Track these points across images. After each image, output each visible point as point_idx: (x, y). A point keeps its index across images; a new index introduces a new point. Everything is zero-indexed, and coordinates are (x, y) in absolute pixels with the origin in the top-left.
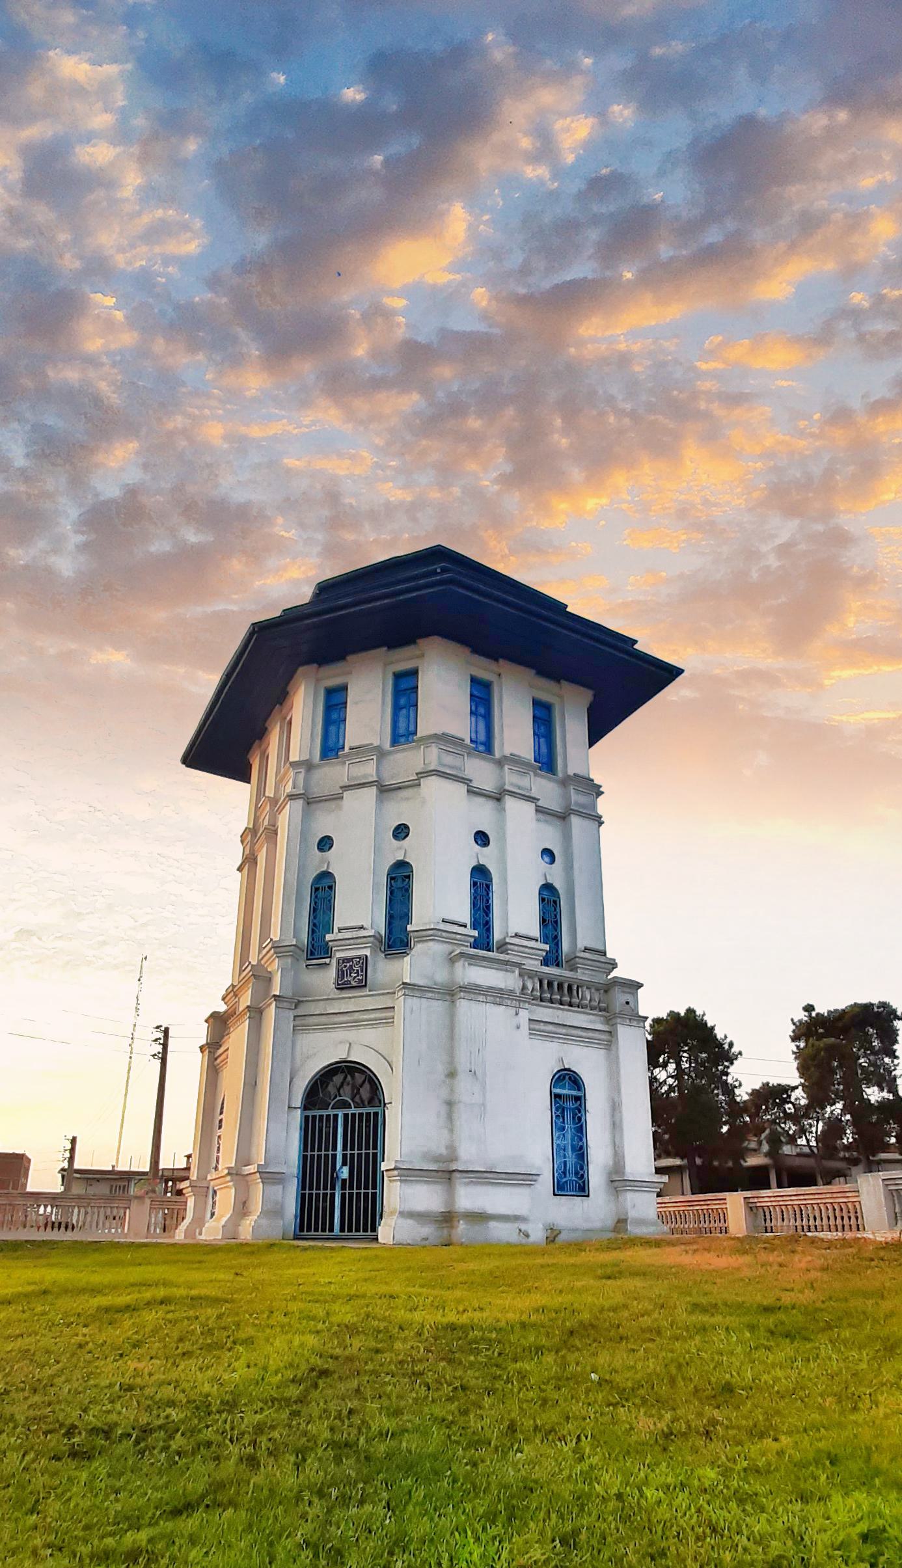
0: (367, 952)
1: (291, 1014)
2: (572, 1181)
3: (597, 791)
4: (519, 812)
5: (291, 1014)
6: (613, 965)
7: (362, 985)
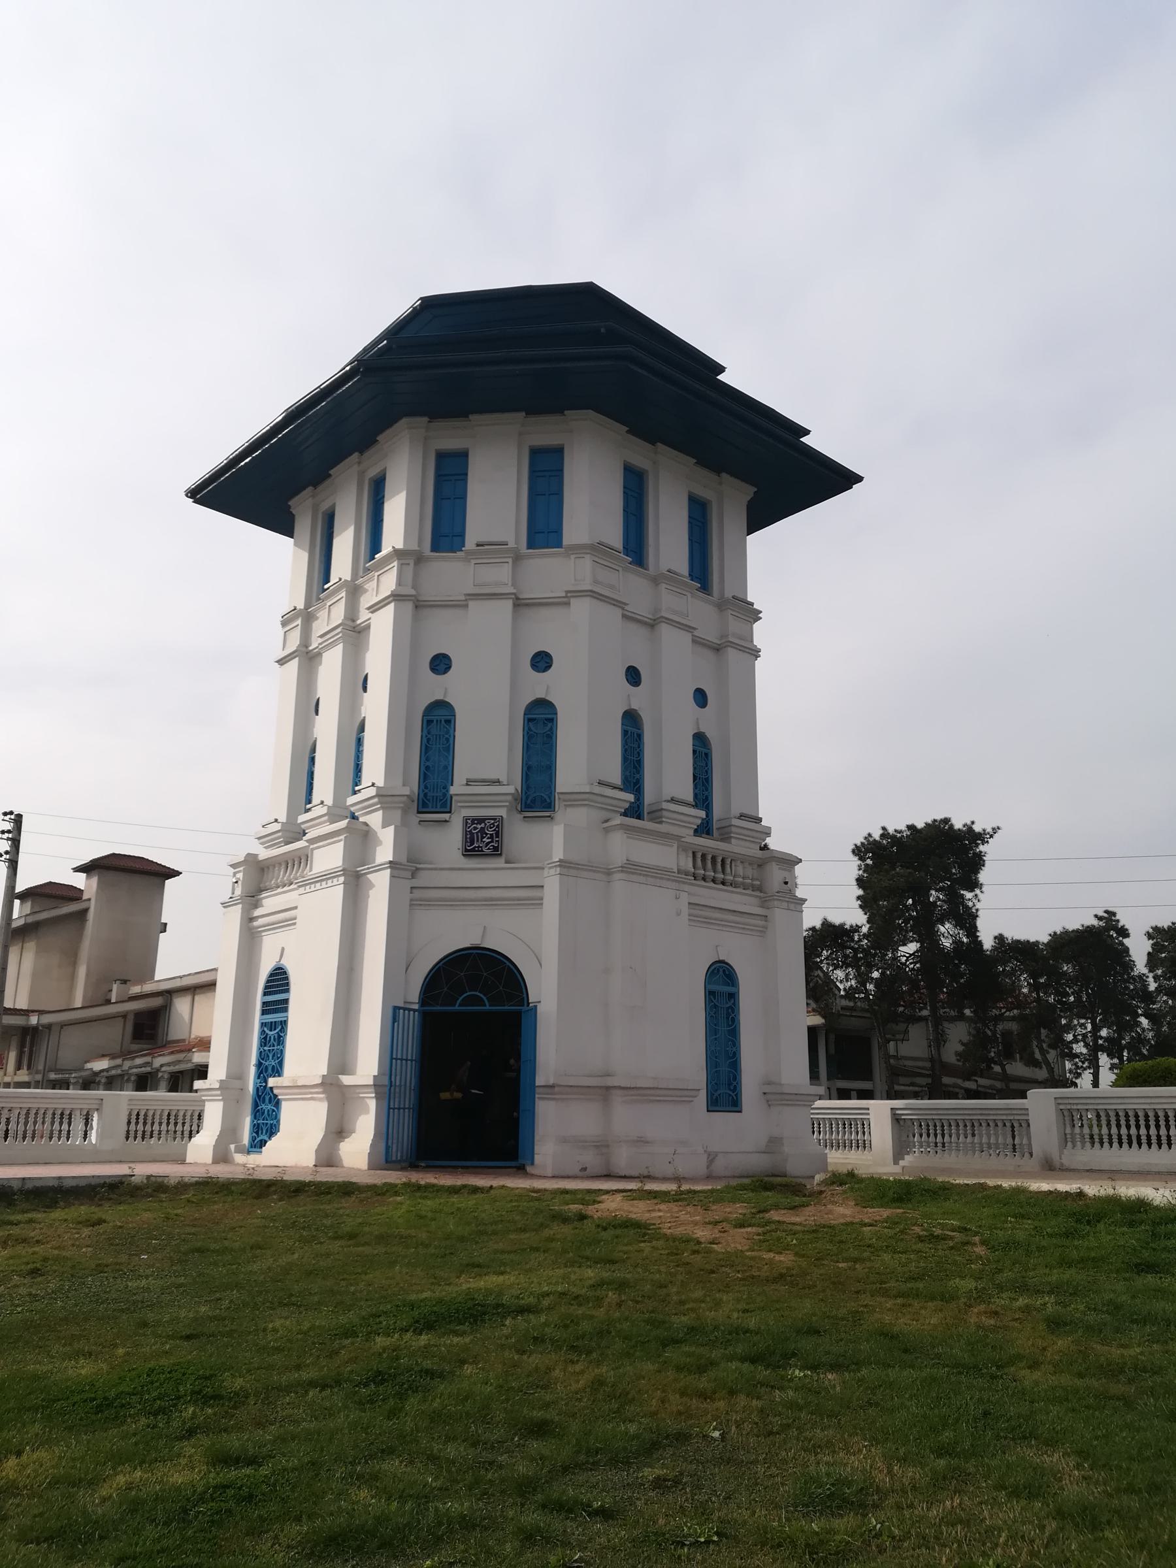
0: (502, 812)
1: (408, 884)
2: (724, 1091)
3: (755, 615)
4: (673, 642)
5: (408, 884)
7: (497, 852)
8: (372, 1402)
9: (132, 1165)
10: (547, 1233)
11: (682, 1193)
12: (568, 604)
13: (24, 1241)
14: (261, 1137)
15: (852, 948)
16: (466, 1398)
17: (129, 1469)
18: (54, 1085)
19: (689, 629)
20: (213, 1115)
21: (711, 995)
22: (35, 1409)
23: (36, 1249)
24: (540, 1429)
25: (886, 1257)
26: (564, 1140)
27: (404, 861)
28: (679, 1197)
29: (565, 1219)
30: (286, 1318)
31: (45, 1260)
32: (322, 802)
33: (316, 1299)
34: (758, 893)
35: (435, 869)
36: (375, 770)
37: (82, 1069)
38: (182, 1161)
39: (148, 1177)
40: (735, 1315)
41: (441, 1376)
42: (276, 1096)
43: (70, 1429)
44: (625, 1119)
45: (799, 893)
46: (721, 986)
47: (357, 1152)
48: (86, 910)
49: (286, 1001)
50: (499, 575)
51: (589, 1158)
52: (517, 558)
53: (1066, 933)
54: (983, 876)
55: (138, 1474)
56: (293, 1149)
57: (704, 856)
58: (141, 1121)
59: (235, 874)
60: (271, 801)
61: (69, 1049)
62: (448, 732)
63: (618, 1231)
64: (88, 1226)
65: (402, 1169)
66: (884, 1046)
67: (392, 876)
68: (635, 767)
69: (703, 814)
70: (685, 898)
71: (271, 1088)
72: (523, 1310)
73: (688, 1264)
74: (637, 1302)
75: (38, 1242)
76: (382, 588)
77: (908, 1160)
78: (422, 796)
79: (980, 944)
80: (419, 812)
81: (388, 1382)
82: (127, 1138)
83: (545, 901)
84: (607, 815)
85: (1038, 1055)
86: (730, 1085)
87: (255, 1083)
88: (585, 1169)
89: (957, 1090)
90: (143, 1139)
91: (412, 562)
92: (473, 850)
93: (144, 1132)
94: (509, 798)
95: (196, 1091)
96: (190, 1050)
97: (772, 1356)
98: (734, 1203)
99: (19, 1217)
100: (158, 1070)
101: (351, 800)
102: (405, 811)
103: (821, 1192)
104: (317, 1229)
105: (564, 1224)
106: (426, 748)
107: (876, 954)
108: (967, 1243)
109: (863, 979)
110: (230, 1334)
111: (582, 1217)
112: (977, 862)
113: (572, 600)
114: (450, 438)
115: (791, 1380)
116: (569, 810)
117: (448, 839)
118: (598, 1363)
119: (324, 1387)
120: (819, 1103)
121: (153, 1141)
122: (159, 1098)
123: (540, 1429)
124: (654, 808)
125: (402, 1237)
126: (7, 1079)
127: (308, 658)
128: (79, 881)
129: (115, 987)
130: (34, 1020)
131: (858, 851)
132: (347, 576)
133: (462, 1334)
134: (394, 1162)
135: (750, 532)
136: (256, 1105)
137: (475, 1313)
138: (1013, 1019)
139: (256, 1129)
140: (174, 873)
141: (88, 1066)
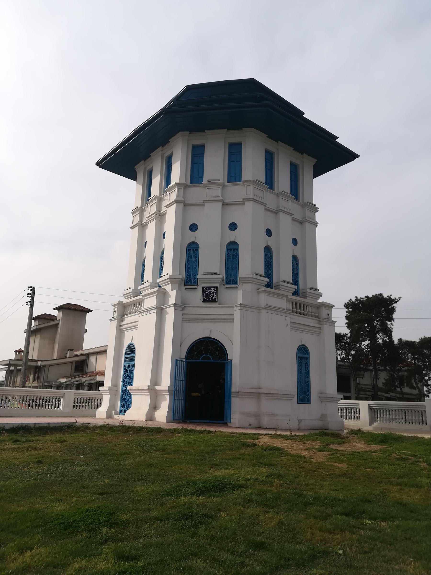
0: (218, 285)
1: (181, 312)
2: (304, 396)
5: (181, 312)
6: (320, 295)
7: (215, 300)
8: (183, 529)
9: (76, 418)
10: (242, 451)
11: (292, 436)
12: (244, 204)
13: (35, 448)
14: (124, 409)
15: (344, 342)
16: (225, 529)
17: (79, 560)
18: (47, 387)
19: (291, 214)
20: (106, 400)
21: (299, 358)
22: (39, 527)
23: (40, 452)
24: (260, 546)
25: (386, 467)
26: (242, 413)
27: (180, 303)
28: (291, 438)
29: (248, 446)
30: (141, 486)
31: (43, 457)
32: (148, 281)
33: (152, 477)
34: (317, 319)
35: (192, 307)
36: (168, 268)
37: (57, 382)
38: (94, 417)
39: (82, 424)
40: (331, 492)
41: (212, 517)
42: (130, 393)
43: (53, 537)
44: (266, 406)
45: (333, 319)
46: (303, 354)
47: (162, 415)
48: (58, 324)
49: (134, 357)
50: (217, 193)
51: (252, 421)
52: (224, 186)
53: (425, 338)
54: (394, 316)
55: (84, 563)
56: (137, 413)
57: (296, 304)
58: (79, 401)
59: (114, 309)
60: (128, 281)
61: (52, 374)
62: (196, 254)
63: (271, 452)
64: (59, 443)
65: (179, 423)
66: (355, 380)
67: (175, 309)
68: (269, 268)
69: (296, 287)
70: (289, 320)
71: (128, 390)
72: (240, 486)
73: (304, 467)
74: (288, 484)
75: (40, 449)
76: (171, 198)
77: (375, 424)
78: (186, 279)
79: (393, 342)
80: (185, 285)
81: (190, 520)
82: (74, 407)
83: (234, 320)
84: (259, 287)
85: (414, 385)
86: (306, 393)
87: (122, 388)
88: (251, 425)
89: (382, 397)
90: (80, 408)
91: (183, 188)
92: (206, 300)
93: (80, 405)
94: (221, 279)
95: (100, 391)
96: (96, 376)
97: (355, 512)
98: (315, 441)
99: (33, 439)
100: (84, 383)
101: (159, 280)
102: (180, 285)
103: (348, 437)
104: (149, 446)
105: (243, 446)
106: (188, 260)
107: (353, 345)
108: (418, 462)
109: (348, 354)
110: (119, 493)
111: (255, 445)
112: (393, 310)
113: (245, 203)
114: (197, 140)
115: (366, 525)
116: (244, 285)
117: (197, 295)
118: (278, 513)
119: (162, 521)
120: (341, 401)
121: (84, 408)
122: (84, 393)
123: (260, 546)
124: (277, 284)
125: (183, 451)
126: (30, 385)
127: (142, 226)
128: (55, 313)
129: (68, 352)
130: (39, 364)
131: (346, 306)
132: (157, 194)
133: (217, 497)
134: (177, 420)
135: (314, 177)
136: (122, 396)
137: (220, 487)
138: (405, 371)
139: (122, 406)
140: (90, 311)
141: (59, 380)
